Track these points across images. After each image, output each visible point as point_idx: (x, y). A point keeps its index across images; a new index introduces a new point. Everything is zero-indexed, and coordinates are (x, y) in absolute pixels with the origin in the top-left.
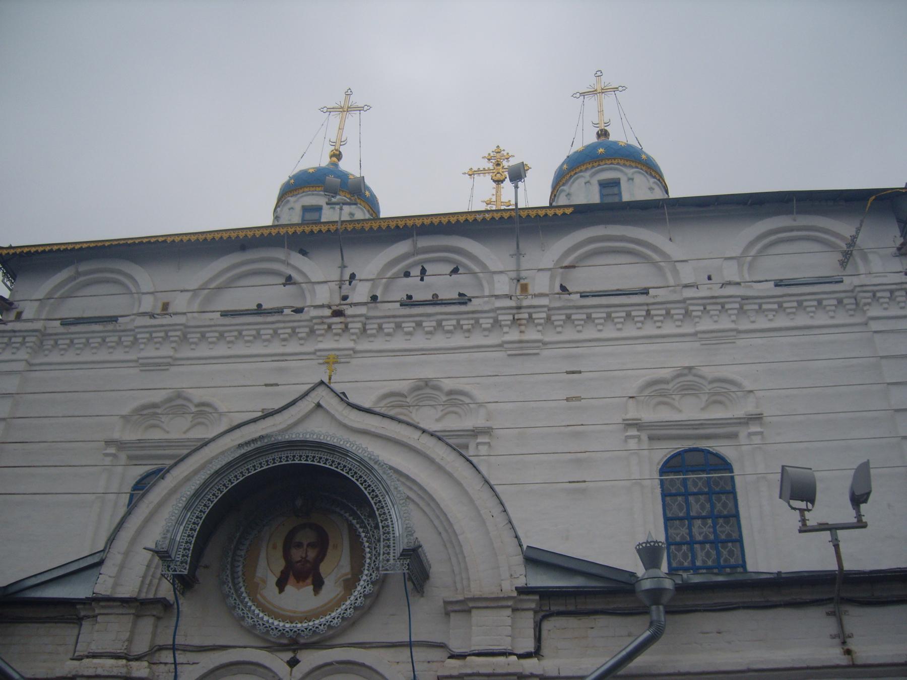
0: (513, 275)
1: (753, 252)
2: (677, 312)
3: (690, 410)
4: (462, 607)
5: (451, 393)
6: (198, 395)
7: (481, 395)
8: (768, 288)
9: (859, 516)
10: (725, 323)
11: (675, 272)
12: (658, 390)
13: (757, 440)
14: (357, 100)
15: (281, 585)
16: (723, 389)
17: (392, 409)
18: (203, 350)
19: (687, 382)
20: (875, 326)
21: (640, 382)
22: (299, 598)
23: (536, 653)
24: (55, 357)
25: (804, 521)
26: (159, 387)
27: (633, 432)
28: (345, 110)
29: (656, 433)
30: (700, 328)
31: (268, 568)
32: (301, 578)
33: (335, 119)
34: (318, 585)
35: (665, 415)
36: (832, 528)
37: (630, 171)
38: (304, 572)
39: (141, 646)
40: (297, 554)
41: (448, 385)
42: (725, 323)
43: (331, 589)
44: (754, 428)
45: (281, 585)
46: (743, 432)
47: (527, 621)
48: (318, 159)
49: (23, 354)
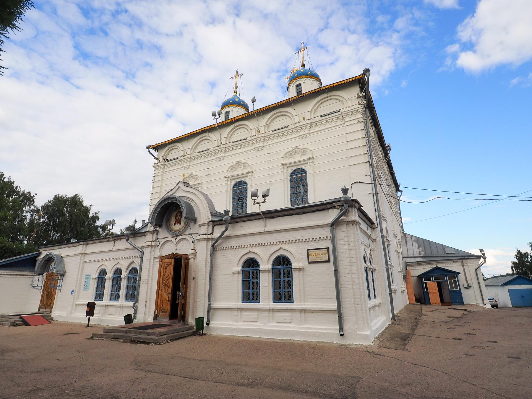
0: (257, 129)
1: (315, 108)
2: (295, 131)
3: (298, 158)
4: (200, 226)
5: (244, 163)
6: (195, 174)
7: (250, 163)
8: (319, 118)
9: (265, 200)
10: (307, 131)
11: (294, 119)
12: (289, 154)
13: (311, 164)
14: (239, 73)
15: (175, 224)
16: (304, 151)
17: (177, 187)
18: (195, 162)
19: (296, 150)
20: (347, 124)
21: (284, 153)
22: (177, 227)
23: (212, 234)
24: (168, 170)
25: (255, 202)
26: (187, 173)
27: (283, 167)
28: (237, 77)
29: (288, 165)
30: (300, 134)
31: (173, 221)
32: (178, 223)
33: (234, 80)
34: (180, 224)
35: (292, 160)
36: (260, 203)
37: (303, 80)
38: (178, 222)
39: (154, 239)
40: (177, 218)
41: (243, 162)
42: (307, 131)
43: (182, 224)
44: (311, 161)
45: (175, 224)
46: (309, 162)
47: (211, 227)
48: (230, 95)
49: (161, 170)
